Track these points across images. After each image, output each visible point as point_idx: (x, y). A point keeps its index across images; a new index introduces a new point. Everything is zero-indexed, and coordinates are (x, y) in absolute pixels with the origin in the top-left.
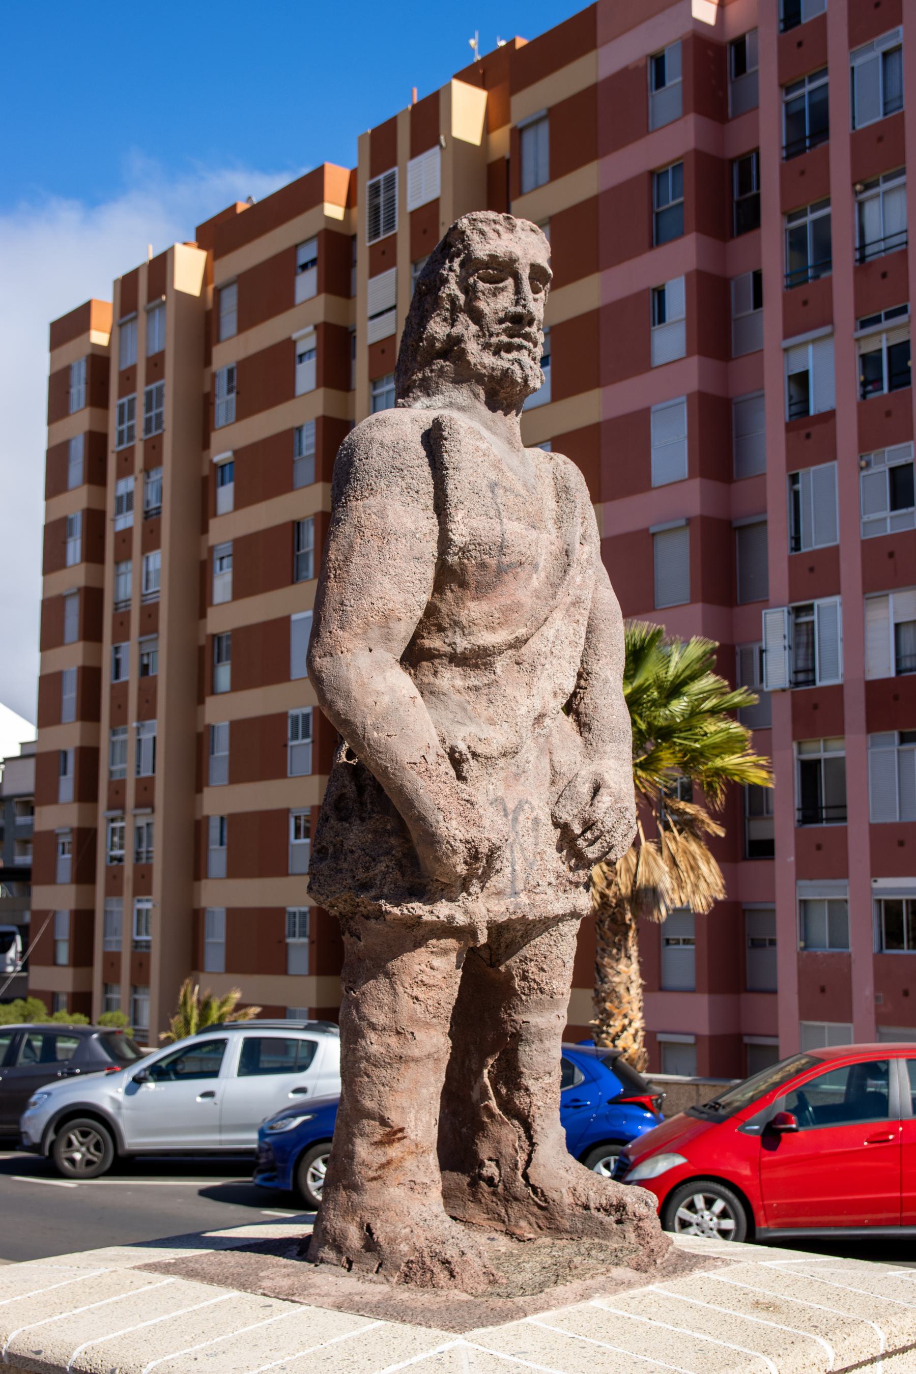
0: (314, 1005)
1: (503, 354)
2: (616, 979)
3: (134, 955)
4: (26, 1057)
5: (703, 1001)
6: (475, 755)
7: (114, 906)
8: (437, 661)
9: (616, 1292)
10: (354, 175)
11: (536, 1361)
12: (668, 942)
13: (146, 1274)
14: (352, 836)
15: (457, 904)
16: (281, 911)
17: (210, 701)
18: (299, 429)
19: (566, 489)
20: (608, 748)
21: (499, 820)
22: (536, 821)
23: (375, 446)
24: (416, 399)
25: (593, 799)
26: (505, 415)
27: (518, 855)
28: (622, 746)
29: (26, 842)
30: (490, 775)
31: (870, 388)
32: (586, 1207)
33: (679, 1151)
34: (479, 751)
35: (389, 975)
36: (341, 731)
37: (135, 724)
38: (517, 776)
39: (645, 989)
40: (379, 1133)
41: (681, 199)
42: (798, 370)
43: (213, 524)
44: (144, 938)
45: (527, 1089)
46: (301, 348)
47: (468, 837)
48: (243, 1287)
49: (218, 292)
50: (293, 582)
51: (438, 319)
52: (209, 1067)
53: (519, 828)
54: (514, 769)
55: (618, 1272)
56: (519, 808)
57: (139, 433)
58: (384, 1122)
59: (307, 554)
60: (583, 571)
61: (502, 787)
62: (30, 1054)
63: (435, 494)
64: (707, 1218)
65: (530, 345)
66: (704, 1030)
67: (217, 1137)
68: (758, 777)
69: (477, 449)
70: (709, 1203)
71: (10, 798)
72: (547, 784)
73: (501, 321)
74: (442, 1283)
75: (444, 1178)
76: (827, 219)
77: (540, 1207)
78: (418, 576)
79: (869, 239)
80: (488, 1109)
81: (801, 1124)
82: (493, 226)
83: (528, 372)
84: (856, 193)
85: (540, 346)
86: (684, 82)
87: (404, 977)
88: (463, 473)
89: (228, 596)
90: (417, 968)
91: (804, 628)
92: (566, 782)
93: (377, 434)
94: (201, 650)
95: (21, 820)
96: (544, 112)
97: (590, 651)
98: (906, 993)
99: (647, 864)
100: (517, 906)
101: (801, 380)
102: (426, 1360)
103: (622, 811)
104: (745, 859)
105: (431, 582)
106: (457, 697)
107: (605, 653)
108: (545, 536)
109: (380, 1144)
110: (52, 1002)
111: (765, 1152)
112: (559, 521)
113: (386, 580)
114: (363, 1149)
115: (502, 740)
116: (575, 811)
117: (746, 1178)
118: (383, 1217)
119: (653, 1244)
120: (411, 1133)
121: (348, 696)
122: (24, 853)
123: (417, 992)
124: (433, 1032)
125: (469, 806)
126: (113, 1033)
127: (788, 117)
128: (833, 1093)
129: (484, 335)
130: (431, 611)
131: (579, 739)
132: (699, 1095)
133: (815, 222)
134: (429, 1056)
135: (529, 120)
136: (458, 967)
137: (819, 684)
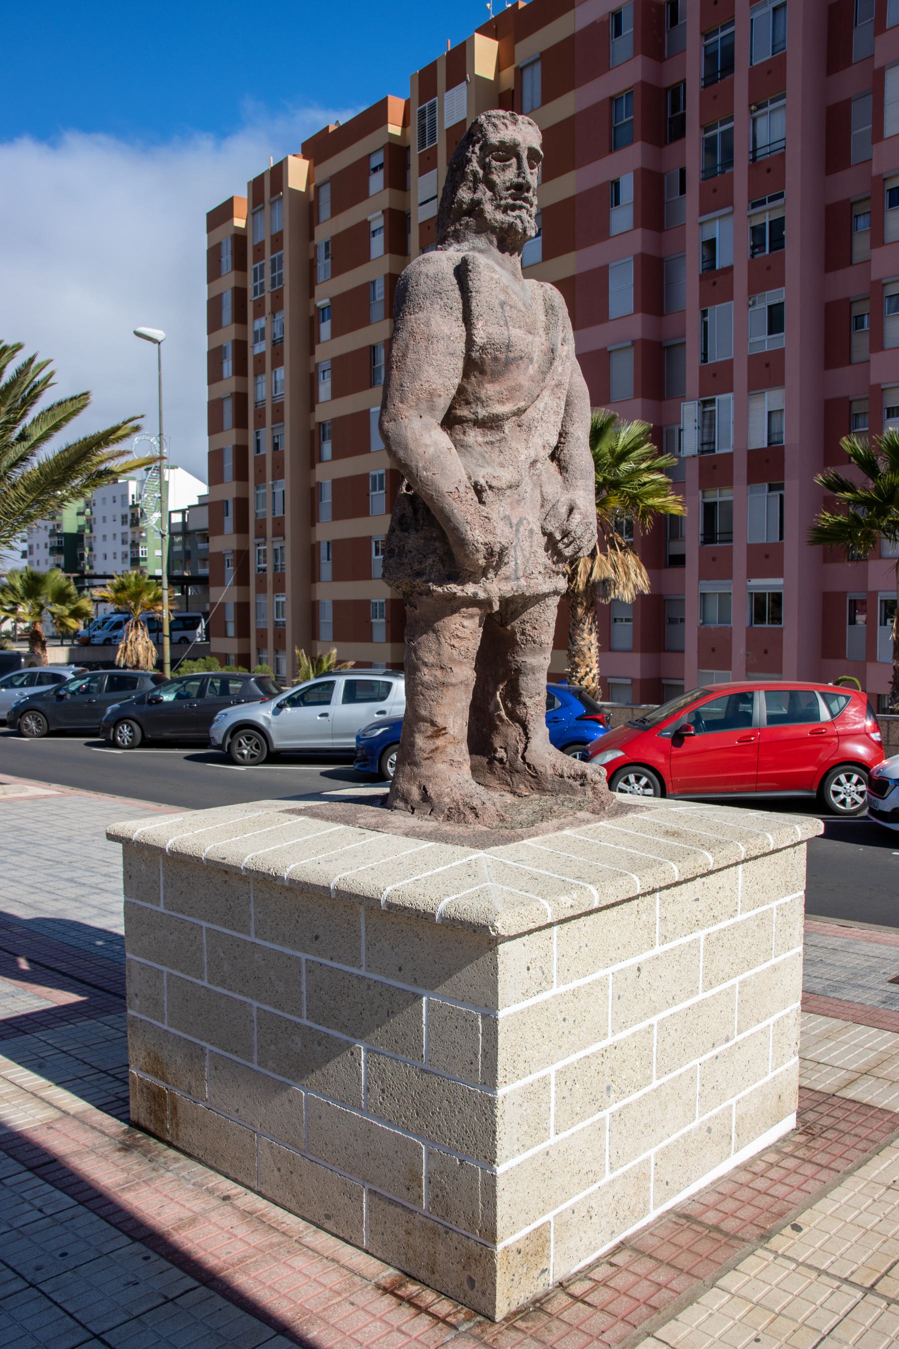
0: (390, 661)
1: (509, 212)
2: (582, 643)
3: (275, 631)
4: (210, 692)
5: (637, 657)
6: (491, 487)
7: (262, 599)
8: (465, 425)
9: (579, 826)
10: (408, 103)
11: (529, 865)
12: (615, 620)
13: (287, 815)
14: (410, 541)
16: (368, 602)
17: (319, 467)
18: (374, 283)
19: (552, 307)
20: (579, 484)
21: (507, 530)
22: (531, 531)
23: (423, 277)
24: (450, 245)
25: (569, 516)
26: (511, 255)
27: (519, 553)
28: (588, 482)
29: (205, 560)
30: (501, 501)
31: (757, 250)
32: (562, 776)
33: (621, 749)
34: (493, 484)
35: (435, 631)
36: (402, 471)
37: (271, 483)
38: (518, 502)
39: (601, 650)
40: (430, 730)
41: (632, 117)
42: (709, 237)
43: (318, 348)
44: (281, 619)
45: (524, 704)
46: (374, 226)
47: (486, 541)
48: (347, 823)
49: (317, 188)
50: (371, 387)
51: (465, 188)
52: (325, 699)
53: (520, 536)
54: (516, 497)
55: (581, 815)
56: (520, 523)
57: (268, 287)
58: (433, 724)
59: (380, 367)
60: (563, 363)
61: (509, 509)
62: (213, 690)
63: (464, 310)
64: (636, 788)
65: (528, 206)
66: (638, 675)
67: (330, 741)
68: (676, 509)
69: (492, 279)
70: (638, 779)
71: (194, 531)
72: (539, 507)
73: (508, 189)
74: (471, 821)
75: (471, 759)
76: (731, 130)
77: (532, 776)
78: (452, 366)
79: (759, 145)
80: (500, 716)
81: (697, 731)
82: (503, 120)
83: (527, 225)
84: (752, 112)
85: (534, 207)
86: (635, 31)
87: (445, 632)
88: (483, 295)
89: (329, 397)
90: (453, 626)
91: (708, 415)
92: (551, 505)
93: (424, 269)
94: (312, 433)
95: (201, 546)
96: (538, 56)
97: (568, 418)
98: (766, 652)
99: (600, 566)
100: (519, 587)
101: (711, 245)
102: (461, 865)
103: (588, 525)
104: (666, 567)
105: (461, 370)
106: (478, 449)
108: (537, 339)
109: (431, 737)
110: (224, 659)
111: (673, 748)
112: (547, 329)
113: (430, 369)
114: (420, 741)
115: (509, 477)
116: (557, 525)
117: (662, 764)
118: (434, 782)
119: (603, 798)
120: (451, 730)
121: (406, 448)
122: (204, 567)
123: (453, 642)
124: (464, 668)
126: (264, 677)
127: (706, 56)
128: (718, 713)
129: (496, 199)
130: (461, 390)
131: (560, 477)
132: (633, 715)
133: (722, 133)
134: (461, 683)
135: (528, 62)
136: (480, 626)
137: (717, 452)
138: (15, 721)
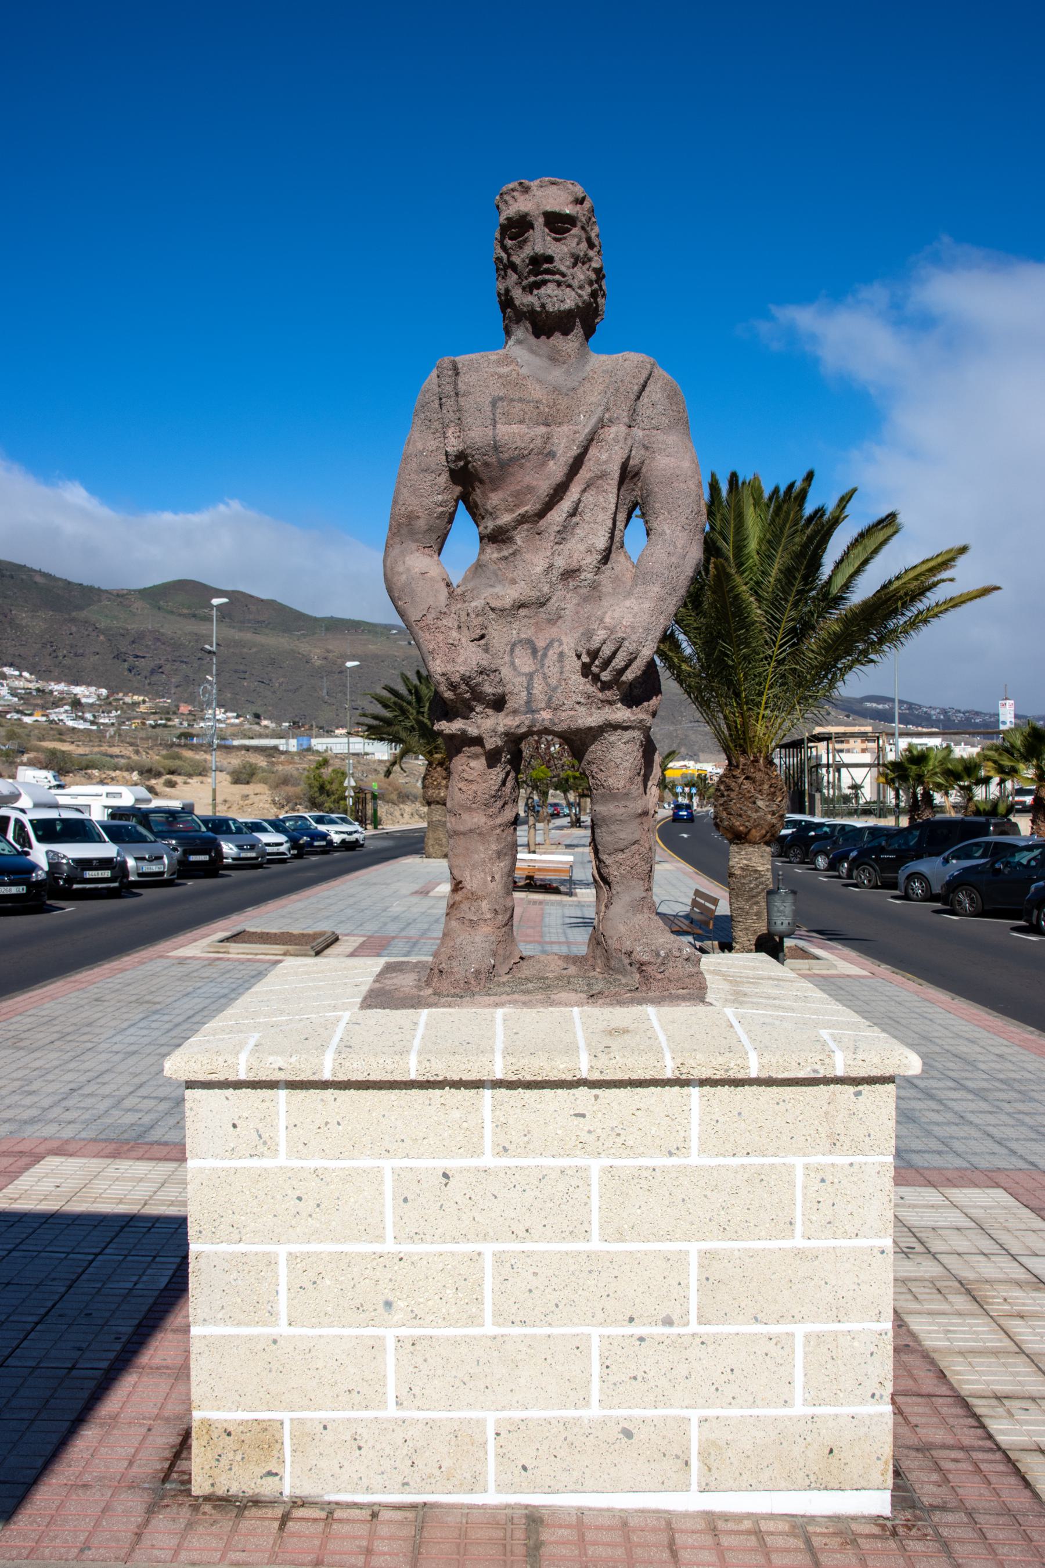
22: (561, 655)
26: (548, 338)
30: (510, 622)
138: (947, 896)
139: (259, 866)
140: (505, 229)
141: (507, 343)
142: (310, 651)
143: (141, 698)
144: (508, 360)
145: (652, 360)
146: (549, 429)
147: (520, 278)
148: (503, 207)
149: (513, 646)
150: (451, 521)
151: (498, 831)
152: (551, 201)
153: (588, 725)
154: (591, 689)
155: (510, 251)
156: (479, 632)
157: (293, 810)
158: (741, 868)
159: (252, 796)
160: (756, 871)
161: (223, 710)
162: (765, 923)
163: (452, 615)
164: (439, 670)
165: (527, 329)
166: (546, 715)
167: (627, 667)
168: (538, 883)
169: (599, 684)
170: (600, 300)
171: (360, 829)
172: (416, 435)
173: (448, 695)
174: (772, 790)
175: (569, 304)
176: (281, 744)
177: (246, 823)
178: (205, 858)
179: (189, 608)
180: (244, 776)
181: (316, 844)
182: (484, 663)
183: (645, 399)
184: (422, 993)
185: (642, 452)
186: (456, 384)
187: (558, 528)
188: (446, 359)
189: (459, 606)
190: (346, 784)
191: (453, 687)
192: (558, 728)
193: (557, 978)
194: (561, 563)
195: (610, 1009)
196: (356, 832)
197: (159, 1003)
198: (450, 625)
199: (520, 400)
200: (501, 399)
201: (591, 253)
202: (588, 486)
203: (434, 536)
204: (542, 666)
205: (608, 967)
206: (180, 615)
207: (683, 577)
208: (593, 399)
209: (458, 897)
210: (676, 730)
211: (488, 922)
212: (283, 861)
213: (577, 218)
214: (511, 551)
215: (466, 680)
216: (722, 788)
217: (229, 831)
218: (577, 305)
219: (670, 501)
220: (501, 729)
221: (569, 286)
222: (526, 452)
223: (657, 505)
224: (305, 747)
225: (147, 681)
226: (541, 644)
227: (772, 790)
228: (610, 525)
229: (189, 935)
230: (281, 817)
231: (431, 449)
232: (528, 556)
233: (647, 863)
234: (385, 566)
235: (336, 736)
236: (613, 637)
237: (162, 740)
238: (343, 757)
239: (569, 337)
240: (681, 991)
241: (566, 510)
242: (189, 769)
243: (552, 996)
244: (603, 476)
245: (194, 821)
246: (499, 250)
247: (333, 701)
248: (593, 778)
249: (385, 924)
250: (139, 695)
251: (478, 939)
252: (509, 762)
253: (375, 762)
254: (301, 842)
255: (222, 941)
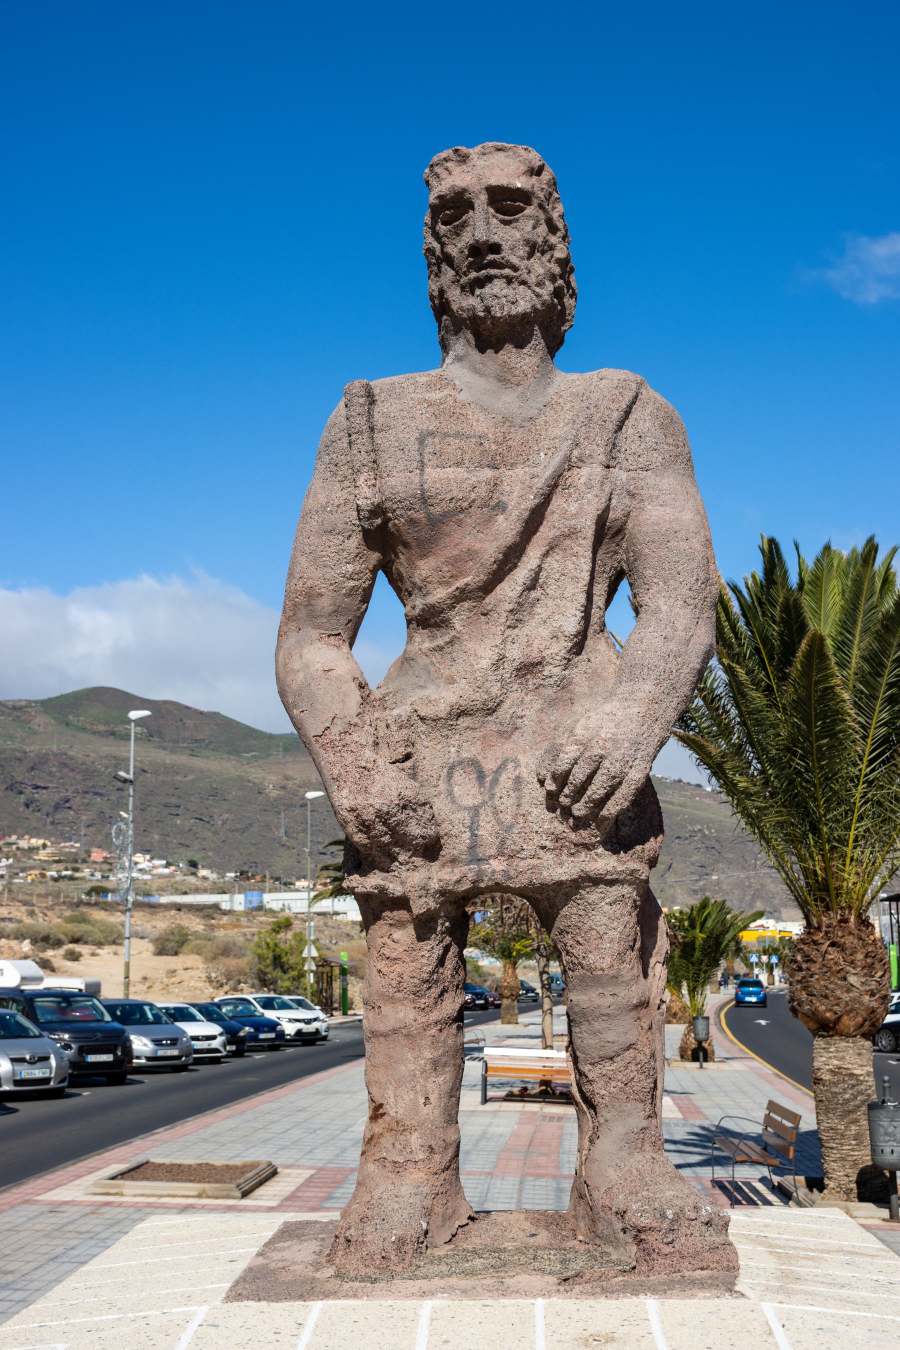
15: (393, 874)
22: (518, 780)
26: (497, 352)
30: (447, 737)
107: (655, 580)
125: (366, 772)
139: (183, 1068)
140: (436, 211)
141: (444, 360)
142: (264, 778)
143: (41, 842)
144: (443, 382)
145: (639, 378)
146: (496, 473)
147: (457, 274)
148: (433, 182)
149: (452, 768)
150: (366, 597)
151: (434, 1031)
152: (497, 171)
153: (556, 878)
154: (560, 828)
155: (444, 239)
156: (402, 751)
157: (235, 989)
158: (831, 1071)
159: (181, 972)
160: (852, 1075)
161: (148, 857)
162: (868, 1151)
163: (366, 728)
164: (347, 804)
165: (468, 341)
166: (497, 865)
167: (608, 796)
168: (558, 1090)
169: (571, 821)
170: (568, 302)
171: (322, 1015)
172: (318, 484)
173: (359, 838)
174: (869, 960)
175: (523, 306)
176: (223, 901)
177: (167, 1009)
178: (107, 1058)
179: (107, 723)
180: (170, 945)
181: (262, 1036)
182: (409, 793)
183: (629, 429)
184: (318, 1275)
185: (627, 501)
186: (370, 415)
187: (511, 607)
188: (356, 383)
189: (376, 715)
190: (305, 954)
191: (365, 827)
192: (515, 884)
193: (520, 1251)
194: (515, 654)
195: (591, 1302)
196: (316, 1020)
197: (12, 1272)
198: (363, 741)
199: (457, 435)
200: (432, 434)
201: (553, 239)
202: (552, 548)
203: (343, 620)
204: (492, 796)
205: (595, 1234)
206: (94, 733)
207: (685, 670)
208: (558, 432)
209: (378, 1128)
210: (748, 878)
211: (420, 1165)
212: (216, 1061)
213: (533, 193)
214: (447, 639)
215: (383, 817)
216: (799, 958)
217: (144, 1020)
218: (533, 306)
219: (667, 566)
220: (434, 885)
221: (524, 283)
222: (465, 504)
223: (649, 572)
224: (255, 904)
225: (50, 819)
226: (489, 766)
227: (869, 960)
228: (583, 601)
229: (71, 1169)
230: (216, 1000)
231: (337, 502)
232: (470, 645)
233: (648, 1076)
234: (276, 661)
235: (297, 890)
236: (587, 754)
237: (67, 896)
238: (306, 918)
239: (525, 351)
240: (699, 1273)
241: (521, 581)
242: (99, 936)
243: (506, 1280)
244: (572, 534)
245: (94, 1007)
246: (430, 239)
247: (292, 843)
248: (568, 953)
249: (344, 1150)
250: (38, 836)
251: (405, 1190)
252: (449, 932)
253: (347, 924)
254: (242, 1034)
255: (113, 1178)
